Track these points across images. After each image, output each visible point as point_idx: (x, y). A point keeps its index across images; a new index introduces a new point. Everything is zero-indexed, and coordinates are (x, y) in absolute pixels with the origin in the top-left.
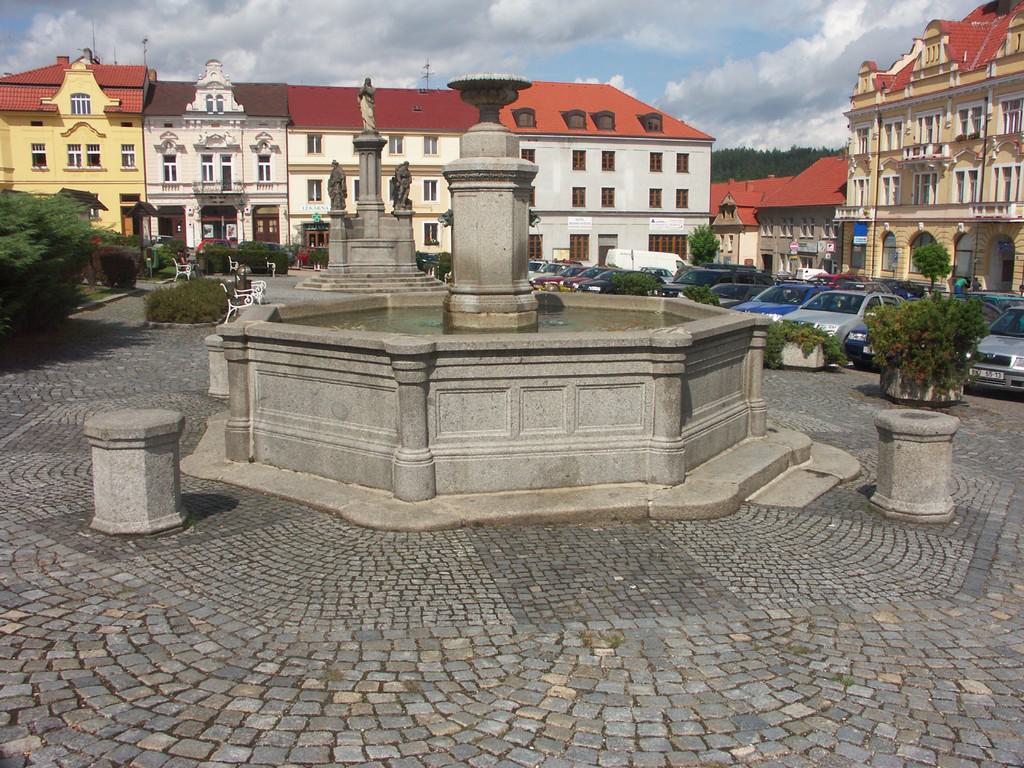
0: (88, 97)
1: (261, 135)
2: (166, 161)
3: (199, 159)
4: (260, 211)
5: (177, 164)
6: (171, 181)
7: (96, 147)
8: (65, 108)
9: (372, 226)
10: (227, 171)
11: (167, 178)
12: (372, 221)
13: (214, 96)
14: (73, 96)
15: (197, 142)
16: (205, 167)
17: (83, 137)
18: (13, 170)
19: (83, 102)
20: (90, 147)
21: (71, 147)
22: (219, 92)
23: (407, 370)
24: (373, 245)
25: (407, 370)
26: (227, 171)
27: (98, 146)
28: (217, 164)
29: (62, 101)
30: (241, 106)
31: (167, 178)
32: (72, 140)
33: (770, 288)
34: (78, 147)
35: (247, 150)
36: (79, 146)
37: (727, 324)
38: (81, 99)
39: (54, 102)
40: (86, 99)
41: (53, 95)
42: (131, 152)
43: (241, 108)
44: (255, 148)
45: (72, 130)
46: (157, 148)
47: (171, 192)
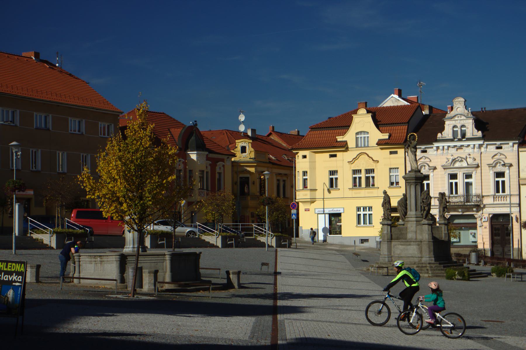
0: (368, 133)
1: (496, 155)
2: (451, 179)
3: (446, 177)
4: (242, 217)
5: (506, 179)
6: (501, 193)
7: (372, 171)
8: (351, 144)
9: (412, 231)
10: (468, 185)
11: (498, 191)
12: (412, 229)
13: (459, 126)
14: (357, 134)
15: (444, 163)
16: (498, 182)
17: (363, 164)
18: (316, 190)
19: (364, 137)
20: (368, 171)
21: (355, 172)
22: (462, 122)
23: (318, 321)
24: (408, 242)
25: (318, 321)
26: (468, 185)
27: (374, 170)
28: (460, 181)
29: (349, 137)
30: (480, 132)
31: (498, 191)
32: (355, 167)
33: (71, 241)
34: (359, 171)
35: (485, 168)
36: (361, 170)
37: (33, 251)
38: (363, 136)
39: (344, 139)
40: (366, 136)
41: (343, 134)
42: (373, 175)
43: (479, 134)
44: (492, 166)
45: (355, 159)
46: (489, 165)
47: (500, 202)
